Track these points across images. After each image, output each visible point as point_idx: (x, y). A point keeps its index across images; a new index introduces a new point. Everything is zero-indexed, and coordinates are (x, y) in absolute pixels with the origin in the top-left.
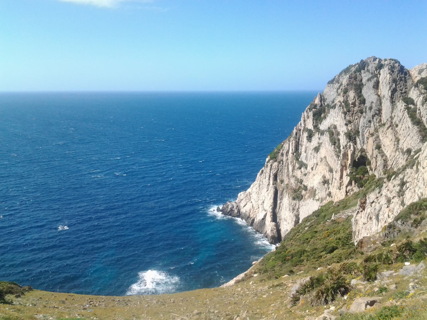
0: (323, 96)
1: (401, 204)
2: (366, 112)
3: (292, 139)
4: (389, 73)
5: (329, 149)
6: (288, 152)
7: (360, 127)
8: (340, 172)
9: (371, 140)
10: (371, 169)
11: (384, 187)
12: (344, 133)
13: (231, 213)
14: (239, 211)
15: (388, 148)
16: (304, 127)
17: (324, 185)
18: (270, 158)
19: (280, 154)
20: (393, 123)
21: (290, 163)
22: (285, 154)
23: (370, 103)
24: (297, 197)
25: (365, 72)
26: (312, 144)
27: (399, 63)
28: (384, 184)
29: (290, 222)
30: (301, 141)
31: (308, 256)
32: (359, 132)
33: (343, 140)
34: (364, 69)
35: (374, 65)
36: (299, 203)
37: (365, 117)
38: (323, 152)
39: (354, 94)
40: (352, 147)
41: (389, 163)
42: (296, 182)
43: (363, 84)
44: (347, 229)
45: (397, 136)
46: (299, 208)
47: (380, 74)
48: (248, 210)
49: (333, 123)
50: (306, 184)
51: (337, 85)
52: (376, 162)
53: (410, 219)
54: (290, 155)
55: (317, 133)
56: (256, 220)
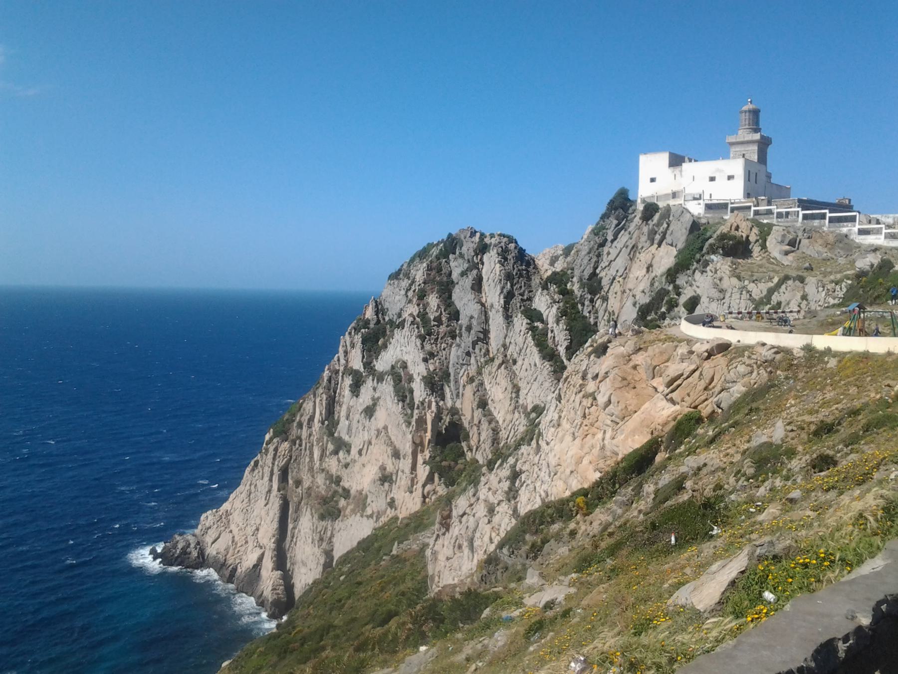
0: (381, 303)
1: (513, 515)
2: (461, 336)
3: (321, 390)
4: (500, 262)
5: (393, 410)
6: (311, 419)
7: (451, 366)
8: (411, 457)
9: (469, 390)
10: (470, 449)
11: (482, 483)
12: (420, 377)
13: (182, 559)
14: (202, 552)
15: (501, 409)
16: (346, 367)
17: (382, 485)
18: (274, 432)
19: (295, 424)
20: (509, 357)
21: (315, 443)
22: (305, 424)
23: (467, 319)
24: (330, 514)
25: (455, 259)
26: (361, 400)
27: (516, 242)
28: (482, 478)
29: (313, 566)
30: (340, 394)
31: (337, 637)
32: (449, 375)
33: (419, 391)
34: (454, 253)
35: (472, 245)
36: (332, 526)
37: (459, 346)
38: (381, 417)
39: (438, 300)
40: (434, 404)
41: (503, 434)
42: (328, 482)
43: (453, 282)
44: (419, 573)
45: (515, 382)
46: (332, 536)
47: (483, 264)
48: (222, 550)
49: (400, 357)
50: (346, 485)
51: (405, 283)
52: (479, 434)
53: (525, 542)
54: (316, 425)
55: (371, 378)
56: (239, 570)
